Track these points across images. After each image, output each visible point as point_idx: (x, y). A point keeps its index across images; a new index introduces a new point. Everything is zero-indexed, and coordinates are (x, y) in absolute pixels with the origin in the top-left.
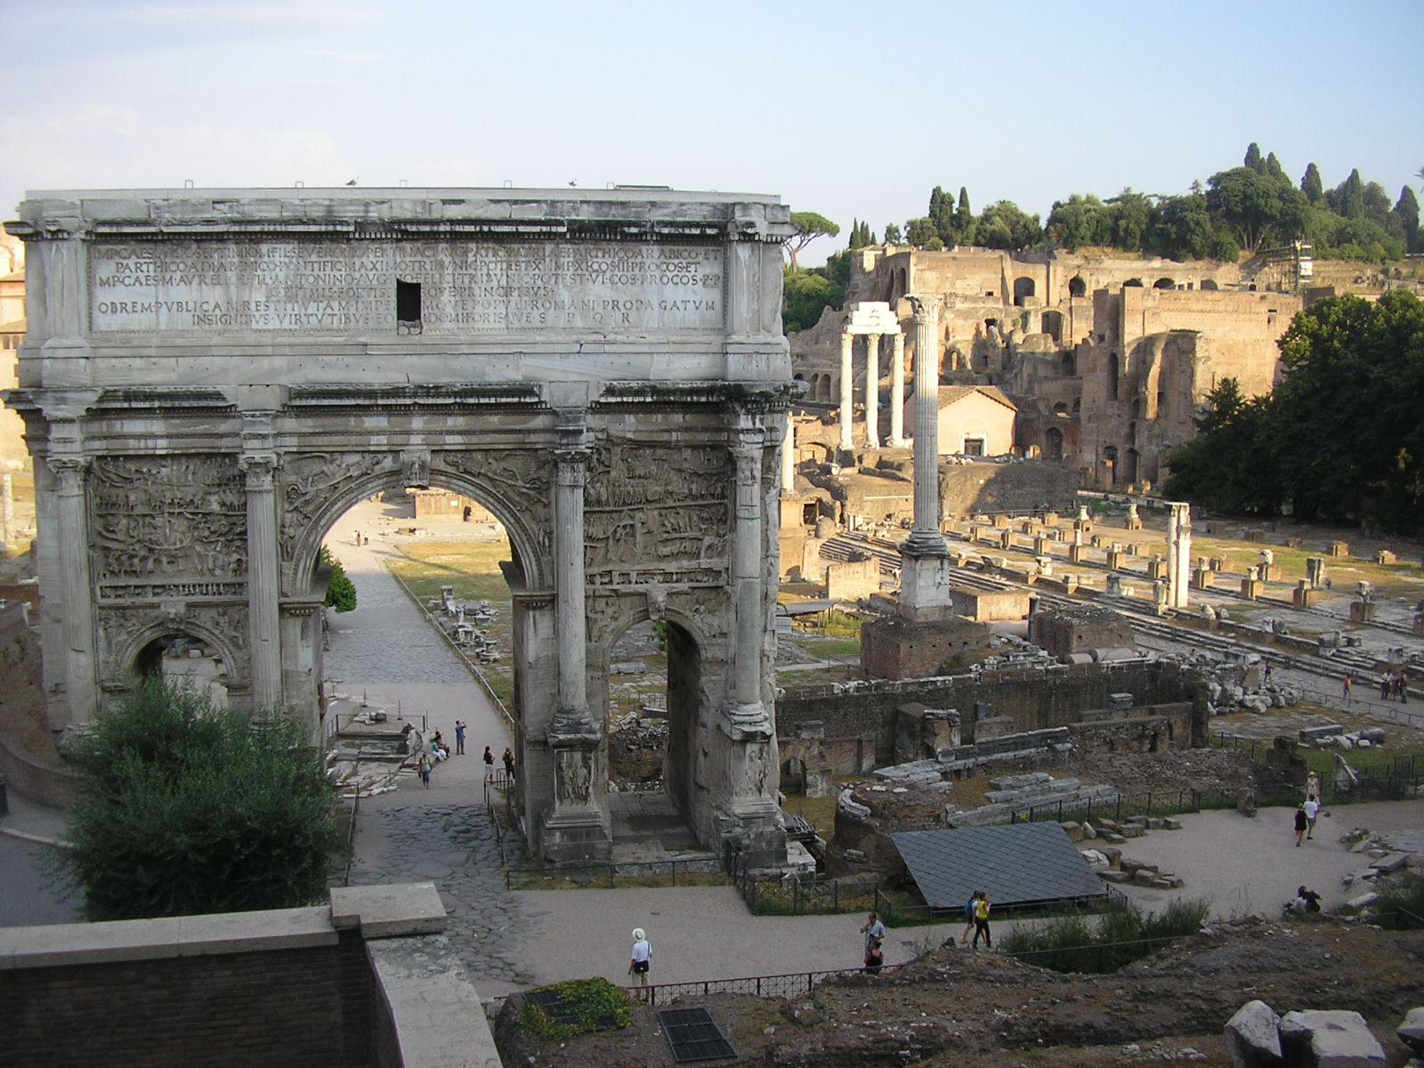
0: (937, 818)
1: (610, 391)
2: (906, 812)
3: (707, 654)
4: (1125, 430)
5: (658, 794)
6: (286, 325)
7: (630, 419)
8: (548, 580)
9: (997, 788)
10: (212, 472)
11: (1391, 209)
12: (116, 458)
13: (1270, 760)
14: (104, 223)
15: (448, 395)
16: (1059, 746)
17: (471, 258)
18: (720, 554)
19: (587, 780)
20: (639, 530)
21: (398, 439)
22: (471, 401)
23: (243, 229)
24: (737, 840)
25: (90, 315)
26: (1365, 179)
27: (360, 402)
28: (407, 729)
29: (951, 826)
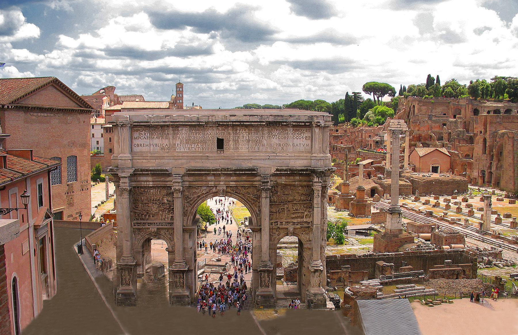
4: (488, 164)
6: (186, 150)
7: (284, 178)
10: (164, 192)
12: (138, 187)
15: (231, 171)
16: (420, 276)
20: (285, 208)
21: (217, 183)
22: (238, 172)
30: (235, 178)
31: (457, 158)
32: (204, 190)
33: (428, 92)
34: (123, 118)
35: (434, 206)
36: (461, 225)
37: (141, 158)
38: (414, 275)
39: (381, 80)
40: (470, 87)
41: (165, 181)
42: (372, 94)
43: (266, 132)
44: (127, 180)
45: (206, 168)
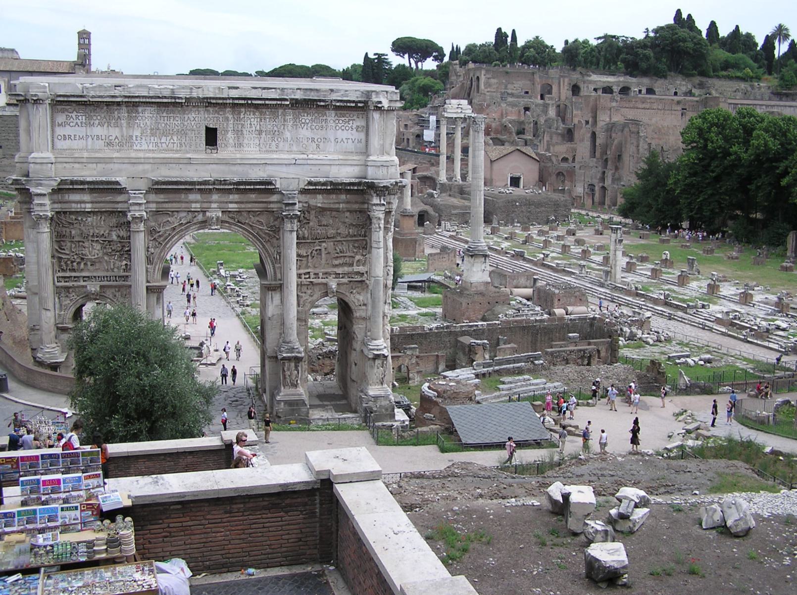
0: (470, 399)
1: (310, 183)
2: (455, 395)
3: (357, 314)
4: (599, 175)
5: (332, 382)
6: (151, 147)
7: (320, 197)
8: (279, 276)
9: (504, 383)
10: (114, 221)
11: (758, 48)
12: (65, 213)
13: (648, 371)
14: (60, 96)
15: (230, 184)
16: (536, 362)
17: (242, 116)
18: (364, 265)
19: (297, 377)
20: (323, 250)
21: (205, 205)
22: (242, 187)
23: (130, 100)
24: (371, 408)
25: (53, 141)
26: (743, 30)
27: (187, 187)
28: (202, 344)
29: (478, 403)
30: (236, 196)
31: (550, 164)
32: (184, 217)
33: (498, 56)
34: (38, 88)
35: (525, 242)
36: (574, 273)
37: (70, 160)
38: (527, 359)
39: (420, 34)
40: (565, 51)
41: (113, 202)
42: (406, 56)
43: (289, 117)
44: (46, 201)
45: (188, 180)
